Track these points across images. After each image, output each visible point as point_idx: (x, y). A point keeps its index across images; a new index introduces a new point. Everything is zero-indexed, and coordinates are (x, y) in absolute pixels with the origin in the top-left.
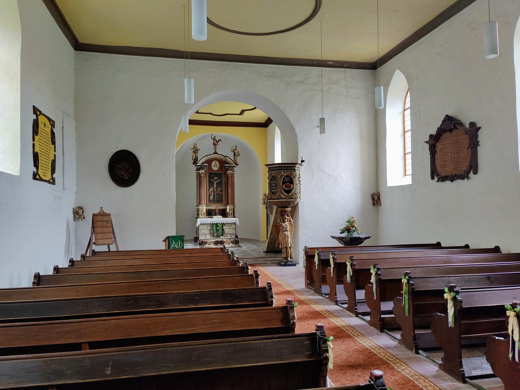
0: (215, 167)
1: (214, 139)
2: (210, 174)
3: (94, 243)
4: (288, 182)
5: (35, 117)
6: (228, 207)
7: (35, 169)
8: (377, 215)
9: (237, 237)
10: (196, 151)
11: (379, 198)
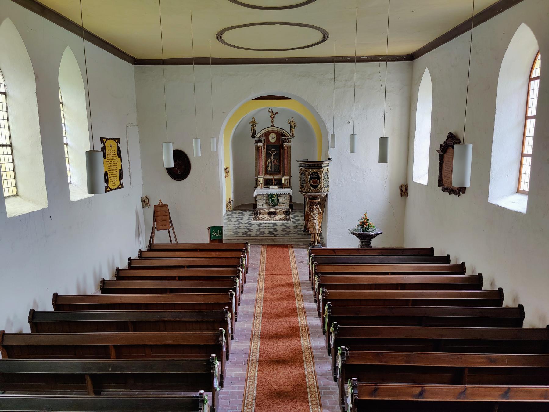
0: (273, 139)
1: (271, 112)
3: (156, 228)
4: (315, 178)
5: (102, 145)
6: (283, 179)
7: (106, 185)
8: (404, 206)
9: (292, 121)
10: (254, 125)
11: (407, 190)
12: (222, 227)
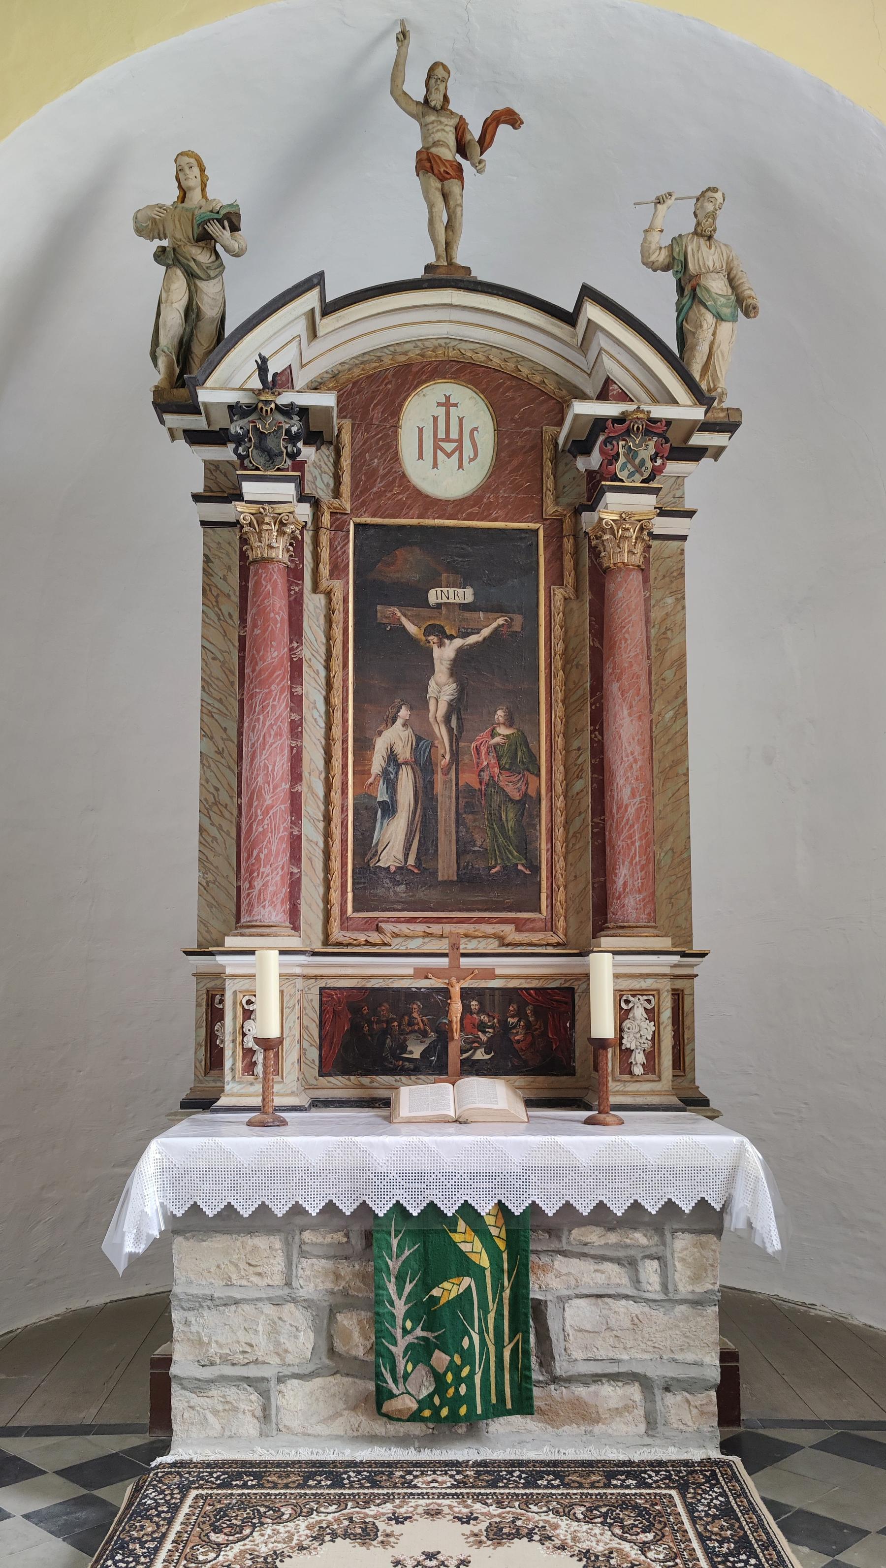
0: (446, 452)
2: (377, 543)
6: (604, 971)
9: (704, 233)
12: (719, 1238)
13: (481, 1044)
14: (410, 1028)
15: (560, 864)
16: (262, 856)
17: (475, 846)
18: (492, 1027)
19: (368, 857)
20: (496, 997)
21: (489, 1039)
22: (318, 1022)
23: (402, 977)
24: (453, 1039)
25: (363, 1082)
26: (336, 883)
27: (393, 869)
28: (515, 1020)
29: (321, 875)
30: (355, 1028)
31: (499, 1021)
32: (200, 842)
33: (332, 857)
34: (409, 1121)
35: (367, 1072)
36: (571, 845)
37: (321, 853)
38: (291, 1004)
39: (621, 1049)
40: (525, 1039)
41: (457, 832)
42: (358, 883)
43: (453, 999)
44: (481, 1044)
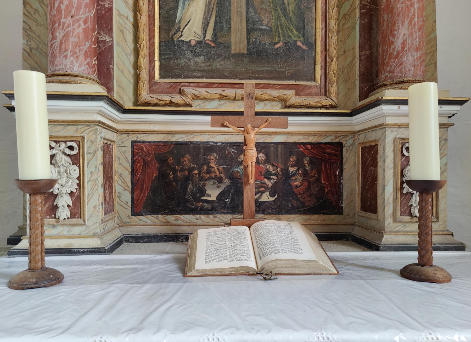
13: (267, 188)
14: (208, 175)
15: (333, 39)
16: (63, 7)
17: (262, 25)
18: (276, 174)
19: (172, 33)
20: (280, 150)
21: (274, 185)
22: (130, 170)
23: (201, 133)
24: (248, 183)
25: (169, 220)
26: (144, 51)
27: (193, 43)
28: (295, 169)
29: (132, 46)
30: (162, 175)
31: (281, 169)
32: (24, 14)
33: (140, 29)
34: (206, 274)
35: (172, 212)
36: (341, 25)
37: (131, 26)
38: (92, 149)
39: (402, 193)
40: (302, 184)
41: (247, 13)
42: (164, 54)
43: (249, 145)
44: (267, 188)
